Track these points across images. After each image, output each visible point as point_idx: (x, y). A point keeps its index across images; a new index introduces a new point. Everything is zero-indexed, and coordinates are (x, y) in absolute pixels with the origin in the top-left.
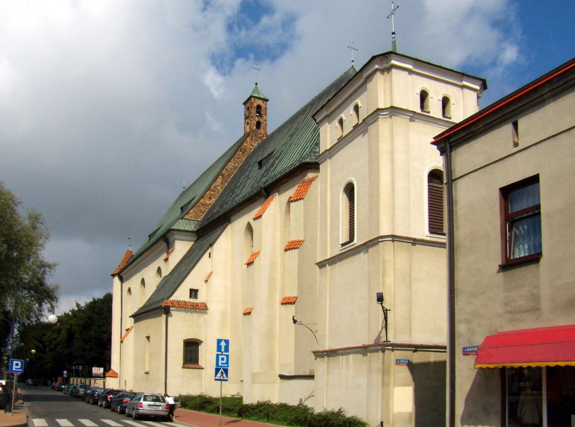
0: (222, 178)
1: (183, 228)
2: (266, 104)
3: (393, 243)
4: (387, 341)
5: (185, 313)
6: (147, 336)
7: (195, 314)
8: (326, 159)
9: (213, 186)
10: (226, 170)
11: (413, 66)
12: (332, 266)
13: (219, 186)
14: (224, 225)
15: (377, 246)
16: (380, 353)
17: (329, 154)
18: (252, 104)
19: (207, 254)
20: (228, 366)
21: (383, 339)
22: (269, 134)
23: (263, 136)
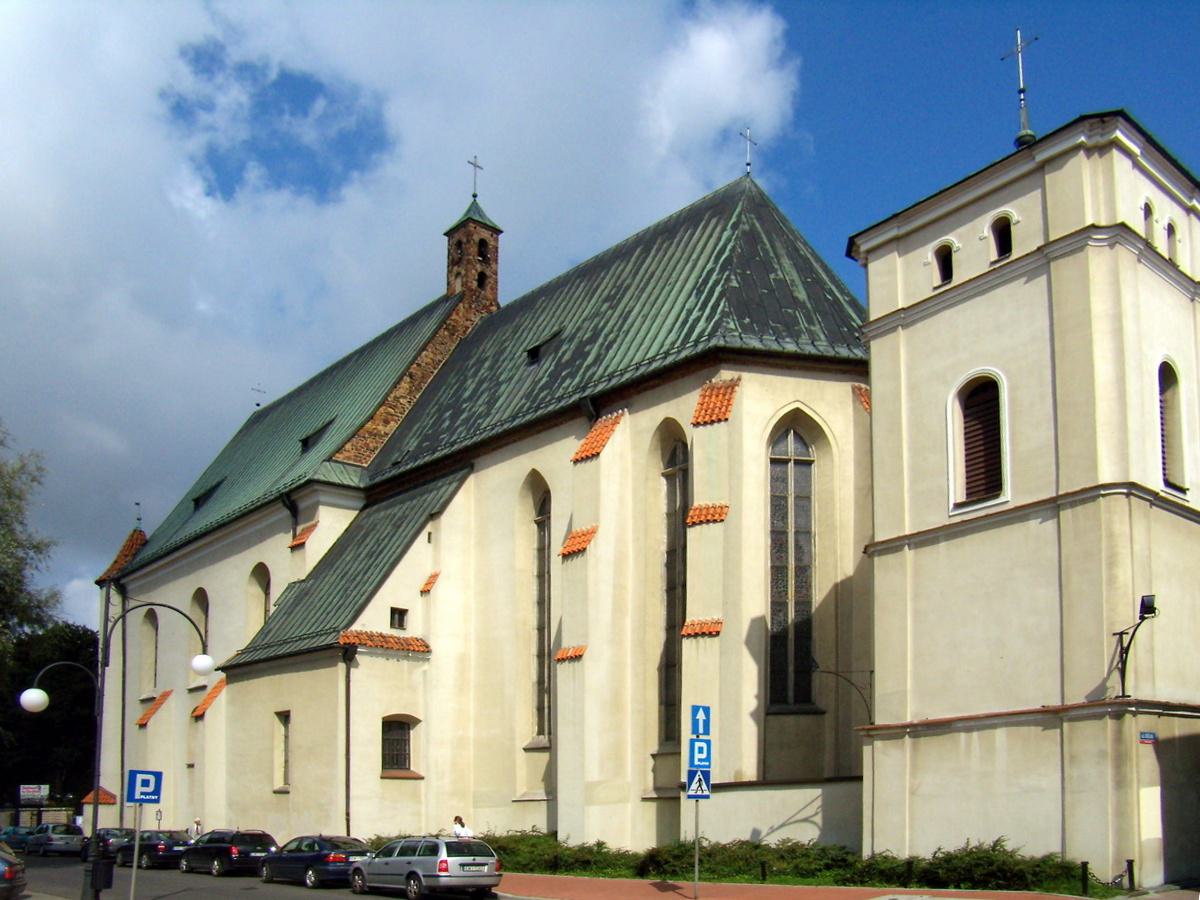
0: (411, 382)
1: (337, 481)
2: (496, 240)
3: (1126, 500)
4: (1124, 696)
5: (384, 659)
6: (280, 709)
7: (405, 664)
8: (898, 326)
9: (392, 395)
10: (419, 365)
11: (1142, 153)
12: (919, 550)
13: (405, 398)
14: (459, 475)
15: (1090, 506)
16: (1109, 723)
17: (904, 318)
18: (469, 235)
19: (423, 536)
20: (709, 766)
21: (1114, 690)
22: (503, 304)
23: (491, 305)
